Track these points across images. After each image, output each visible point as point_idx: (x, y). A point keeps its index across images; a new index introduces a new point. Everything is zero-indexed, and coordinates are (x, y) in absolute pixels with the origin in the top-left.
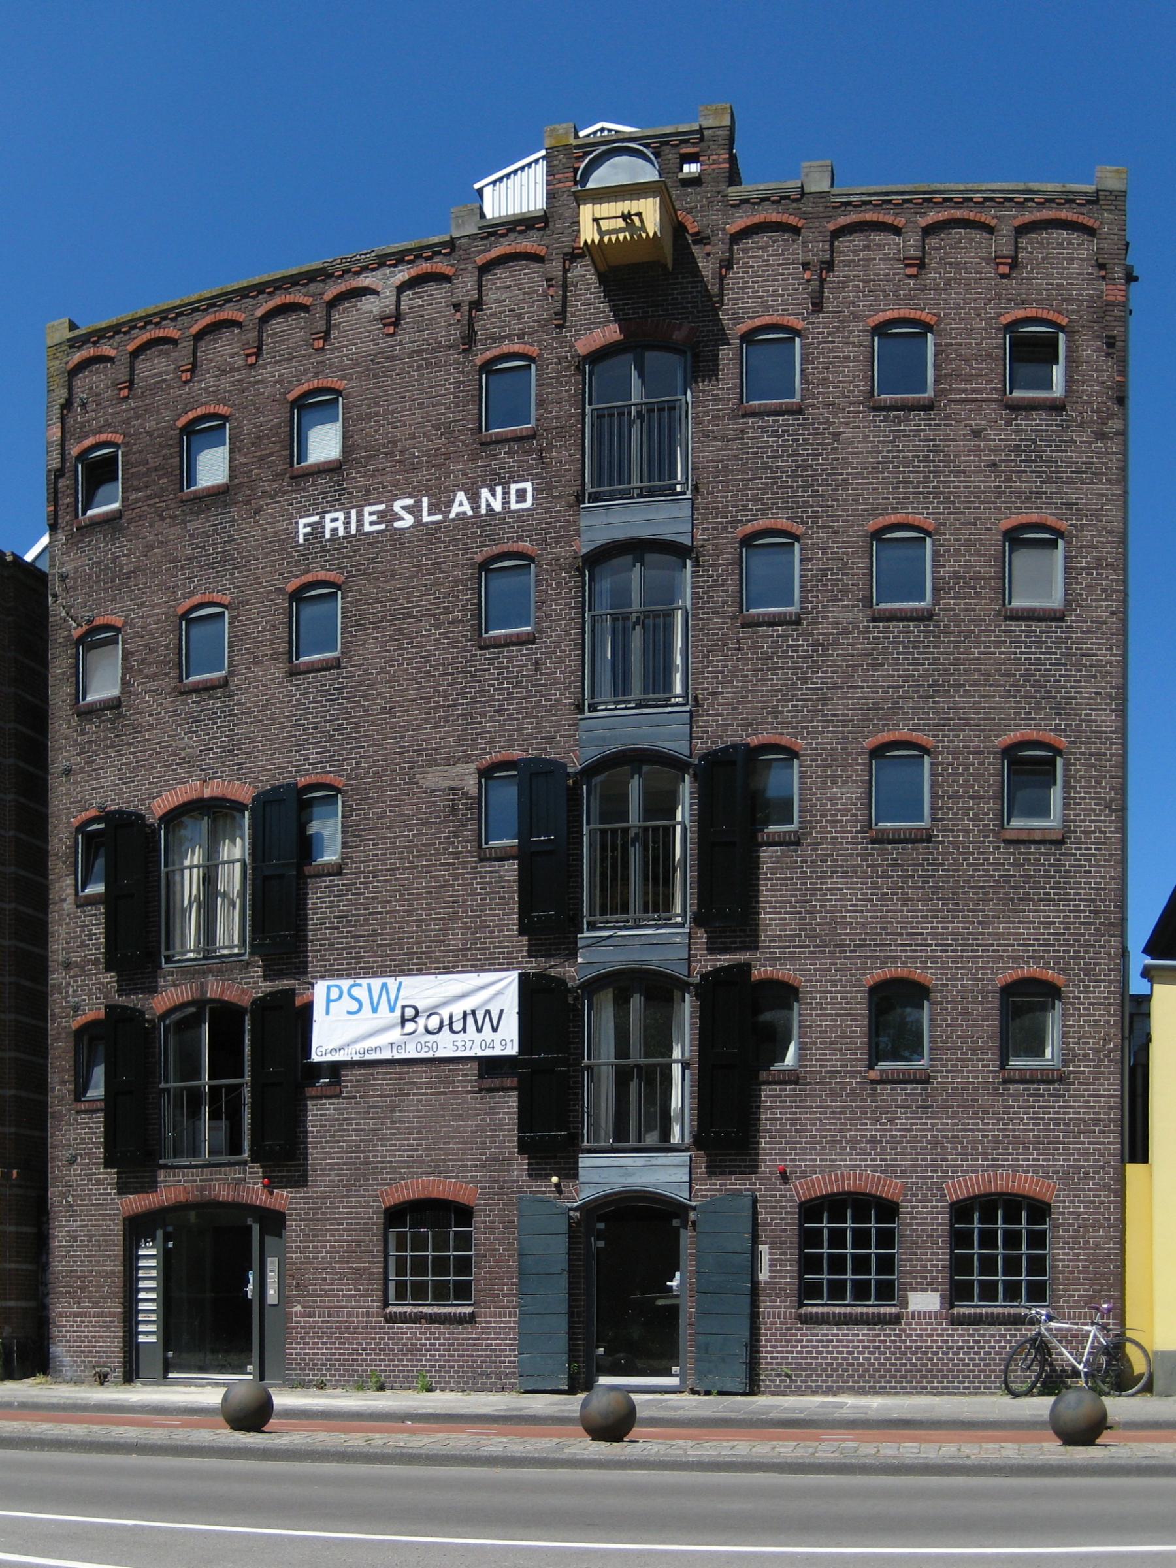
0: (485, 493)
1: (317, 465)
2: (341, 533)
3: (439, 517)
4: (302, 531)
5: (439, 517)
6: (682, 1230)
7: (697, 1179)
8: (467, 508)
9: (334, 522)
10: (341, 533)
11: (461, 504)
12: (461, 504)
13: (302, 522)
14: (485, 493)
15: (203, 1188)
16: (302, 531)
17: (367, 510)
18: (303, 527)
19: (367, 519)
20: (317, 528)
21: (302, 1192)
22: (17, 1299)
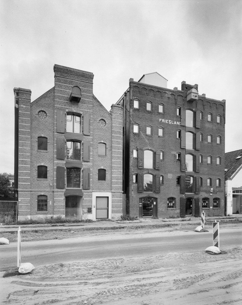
0: (177, 122)
1: (142, 83)
2: (164, 122)
3: (173, 124)
4: (160, 120)
5: (173, 124)
6: (199, 94)
7: (24, 133)
8: (176, 123)
9: (163, 120)
10: (164, 122)
11: (175, 123)
12: (175, 123)
13: (160, 119)
14: (177, 122)
15: (149, 195)
16: (160, 120)
17: (166, 120)
18: (160, 120)
19: (166, 121)
20: (161, 121)
21: (99, 168)
22: (220, 240)
